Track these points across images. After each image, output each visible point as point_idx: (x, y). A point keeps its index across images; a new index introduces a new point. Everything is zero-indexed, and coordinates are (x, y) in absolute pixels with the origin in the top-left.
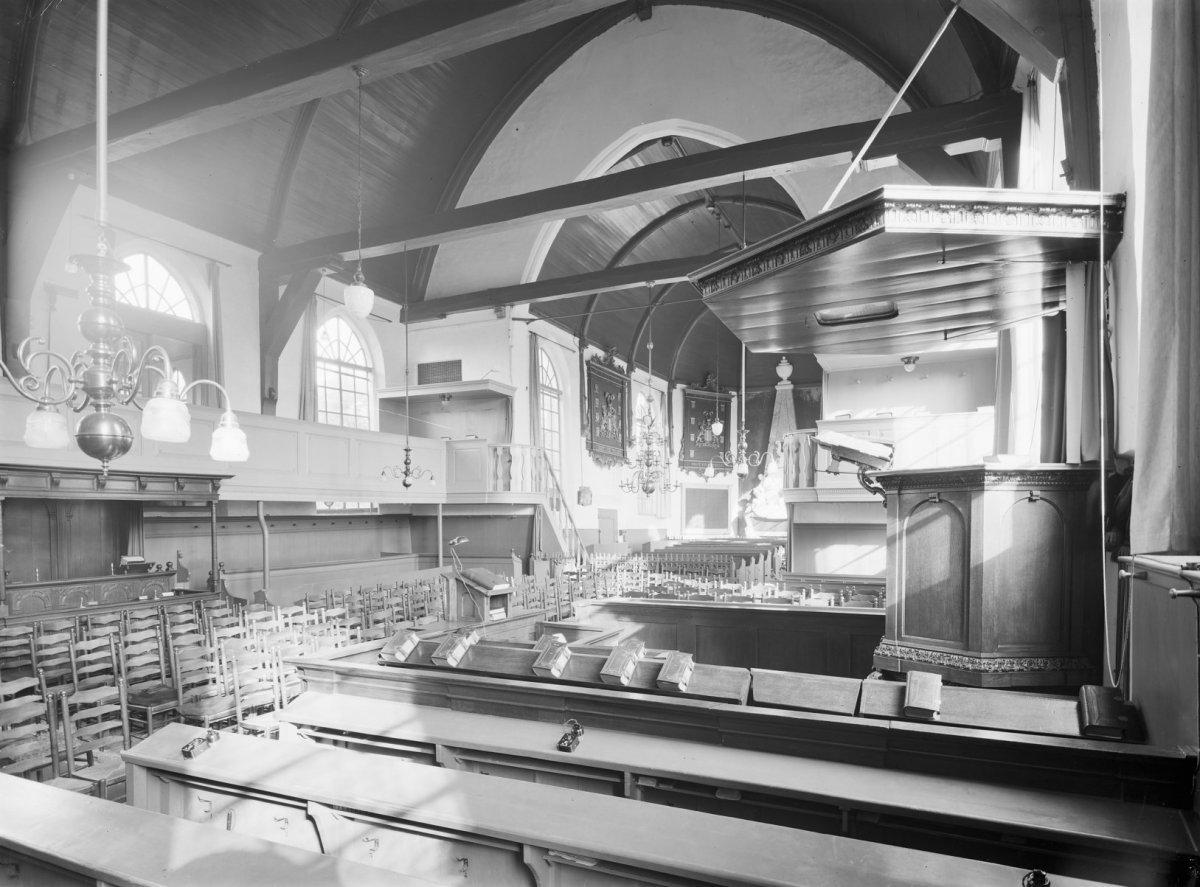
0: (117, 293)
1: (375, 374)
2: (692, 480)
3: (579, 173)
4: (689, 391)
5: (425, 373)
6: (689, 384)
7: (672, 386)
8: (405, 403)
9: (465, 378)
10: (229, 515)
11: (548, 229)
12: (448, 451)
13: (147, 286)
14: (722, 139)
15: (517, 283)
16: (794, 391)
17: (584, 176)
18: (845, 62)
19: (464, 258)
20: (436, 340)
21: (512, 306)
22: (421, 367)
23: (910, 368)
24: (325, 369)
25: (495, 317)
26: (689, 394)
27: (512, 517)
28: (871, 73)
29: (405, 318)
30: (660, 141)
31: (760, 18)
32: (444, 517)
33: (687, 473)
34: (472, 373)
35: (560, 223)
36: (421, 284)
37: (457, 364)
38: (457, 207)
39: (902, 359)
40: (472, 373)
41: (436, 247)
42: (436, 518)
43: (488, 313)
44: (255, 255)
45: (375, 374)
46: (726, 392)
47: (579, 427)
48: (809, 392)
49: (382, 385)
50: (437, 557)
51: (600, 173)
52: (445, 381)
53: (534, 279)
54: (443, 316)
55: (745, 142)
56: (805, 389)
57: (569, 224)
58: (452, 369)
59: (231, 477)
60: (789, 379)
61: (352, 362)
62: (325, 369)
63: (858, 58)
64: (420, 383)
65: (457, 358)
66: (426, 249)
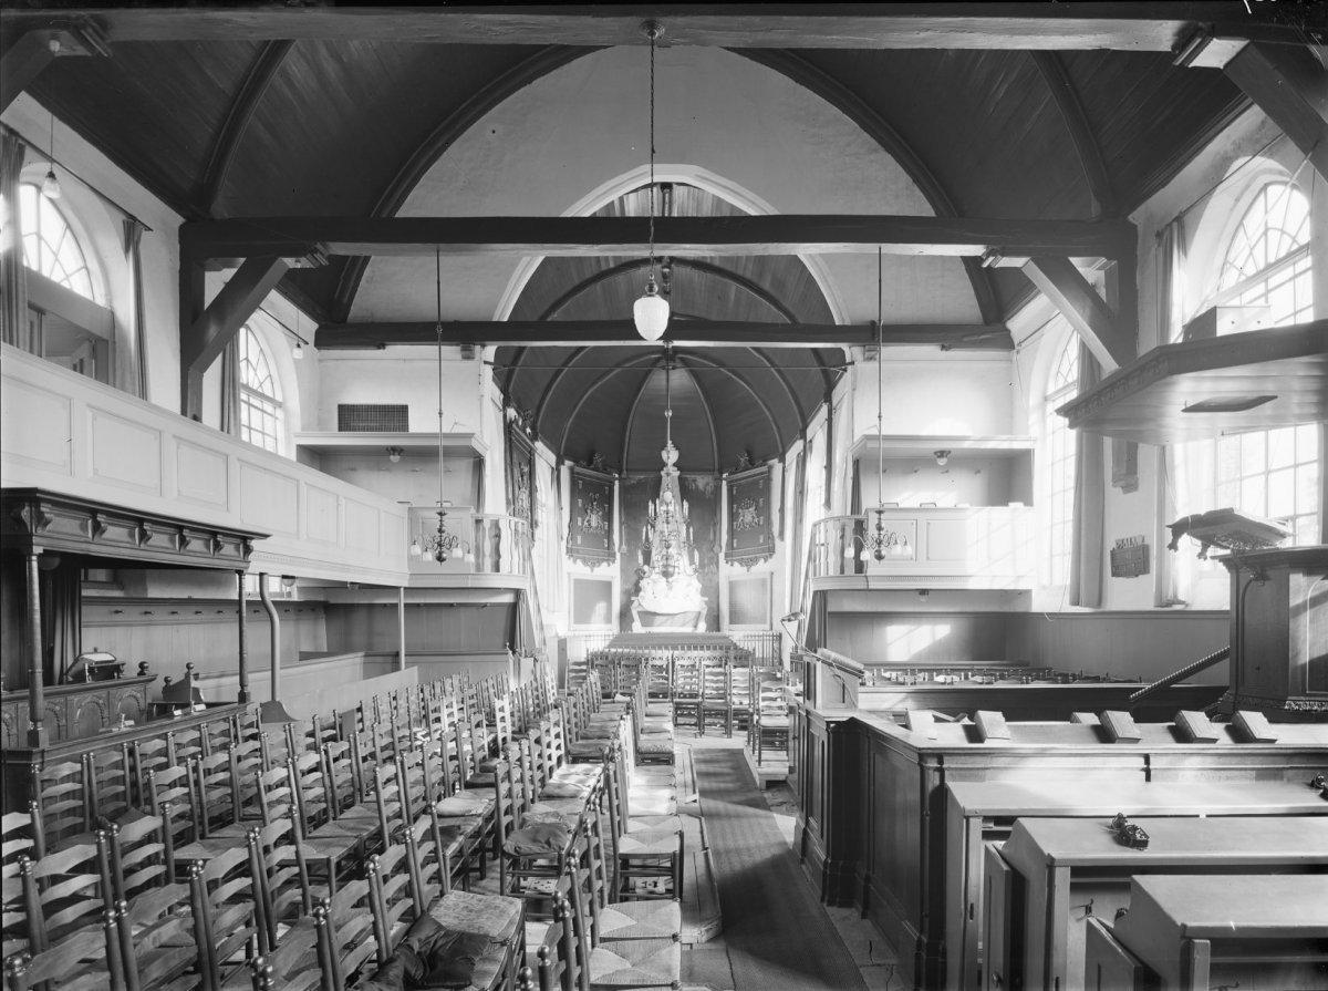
0: (1241, 280)
1: (286, 412)
2: (581, 570)
3: (572, 202)
4: (578, 469)
5: (350, 417)
6: (576, 461)
7: (560, 462)
8: (438, 455)
9: (414, 427)
10: (150, 596)
11: (527, 261)
12: (411, 519)
13: (40, 238)
14: (750, 205)
15: (480, 317)
16: (680, 478)
17: (569, 213)
18: (876, 151)
19: (396, 279)
20: (373, 377)
21: (483, 346)
22: (342, 408)
23: (942, 462)
24: (249, 404)
25: (459, 356)
26: (578, 473)
27: (485, 605)
28: (900, 169)
29: (322, 341)
30: (659, 186)
31: (791, 82)
32: (406, 605)
33: (575, 561)
34: (422, 422)
35: (540, 260)
36: (345, 300)
37: (403, 410)
38: (400, 214)
39: (935, 453)
40: (422, 422)
41: (367, 259)
42: (395, 606)
43: (451, 351)
44: (178, 220)
45: (286, 412)
46: (610, 473)
47: (505, 502)
48: (694, 481)
49: (297, 423)
50: (397, 655)
51: (587, 214)
52: (380, 429)
53: (506, 319)
54: (381, 346)
55: (776, 213)
56: (690, 477)
57: (547, 261)
58: (395, 416)
59: (266, 536)
60: (674, 465)
61: (260, 390)
62: (249, 404)
63: (888, 149)
64: (340, 429)
65: (404, 403)
66: (356, 258)
